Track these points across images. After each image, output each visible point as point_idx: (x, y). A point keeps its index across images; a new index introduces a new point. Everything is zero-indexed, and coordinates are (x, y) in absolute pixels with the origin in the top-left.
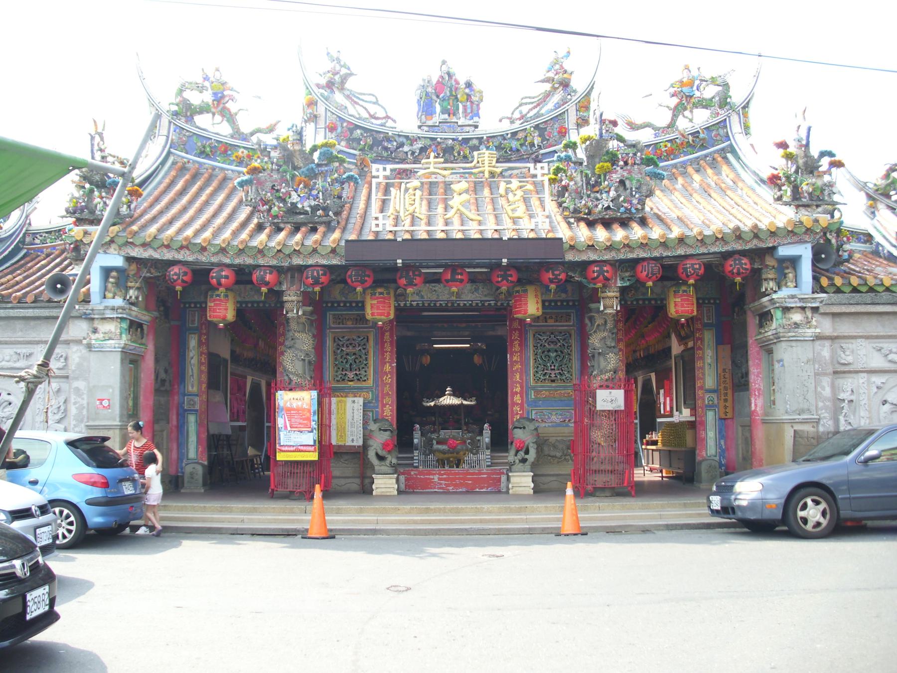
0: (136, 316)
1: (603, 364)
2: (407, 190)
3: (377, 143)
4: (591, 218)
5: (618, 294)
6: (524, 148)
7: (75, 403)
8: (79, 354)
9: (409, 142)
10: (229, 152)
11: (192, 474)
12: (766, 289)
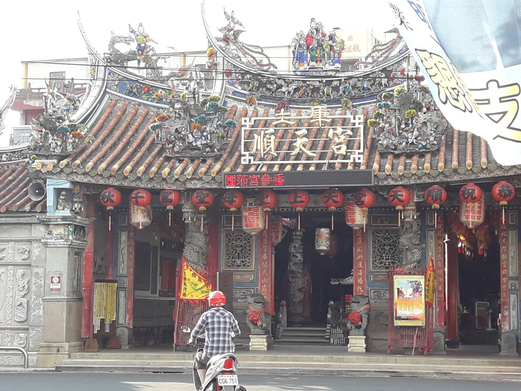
0: (80, 222)
1: (410, 256)
2: (265, 135)
3: (262, 85)
4: (396, 152)
5: (414, 208)
6: (374, 87)
7: (35, 284)
9: (286, 84)
10: (151, 92)
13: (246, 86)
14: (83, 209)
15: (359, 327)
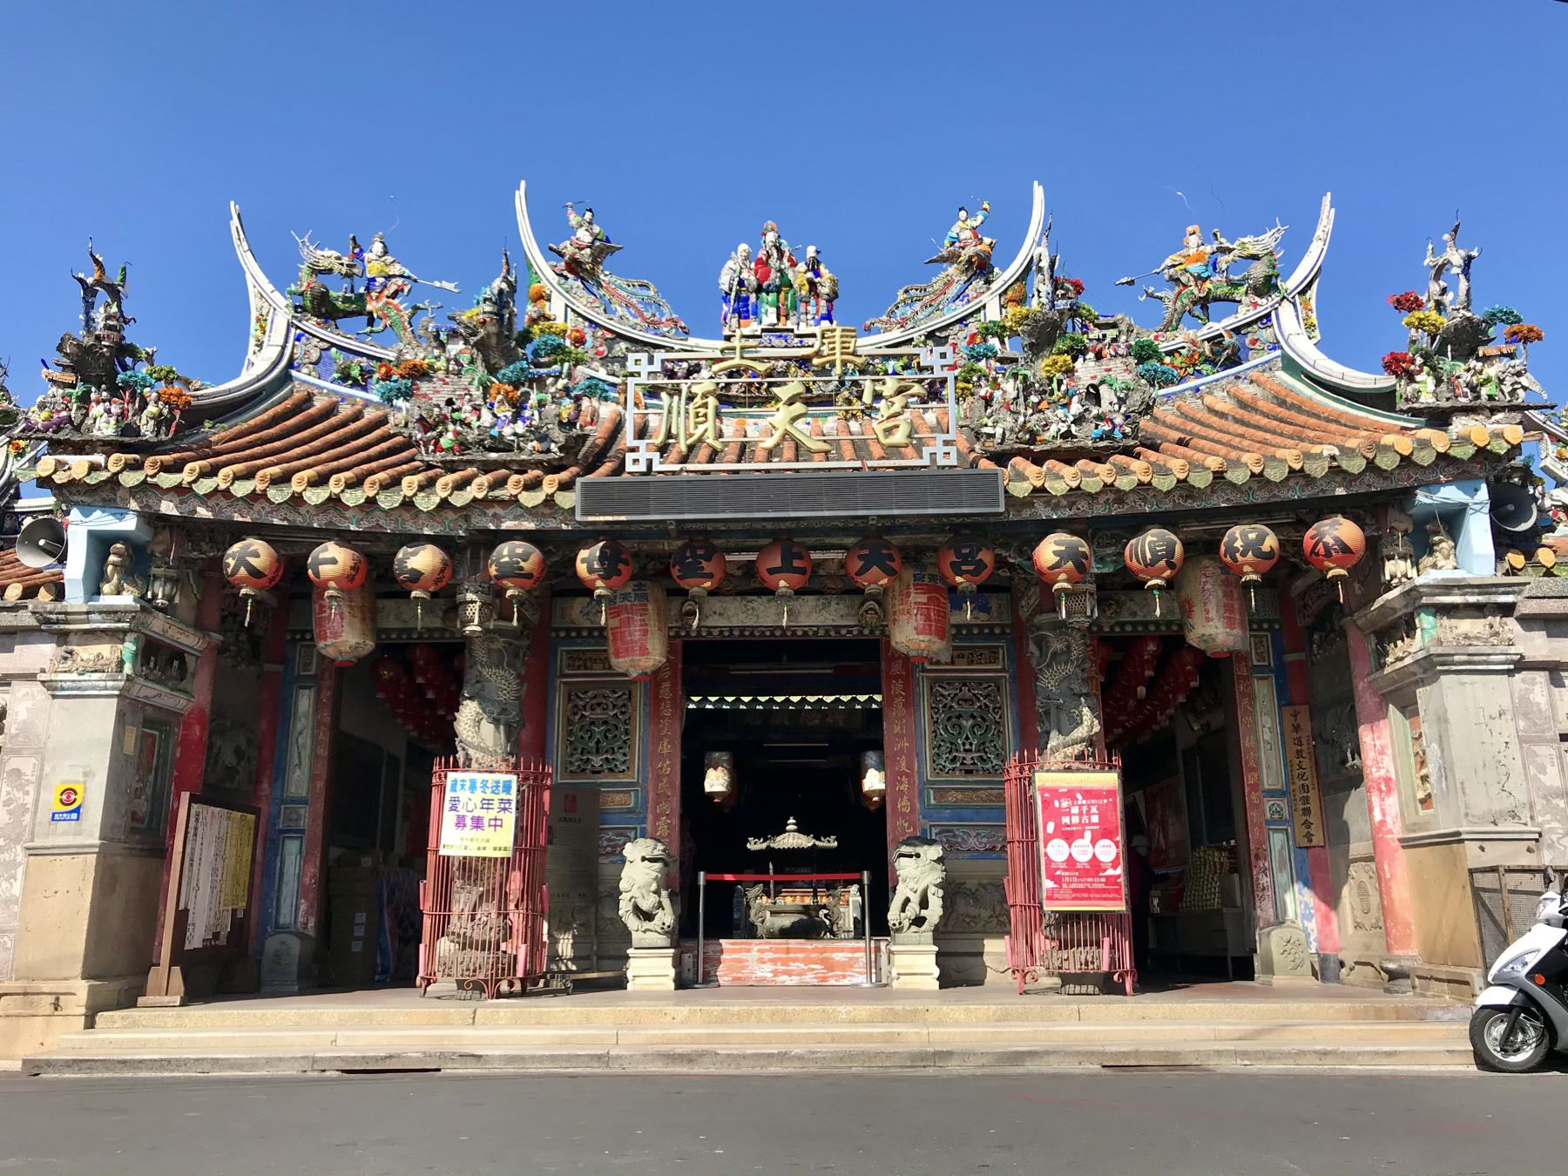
4: (1037, 448)
8: (29, 704)
11: (277, 955)
12: (1393, 577)
13: (616, 367)
14: (177, 600)
15: (919, 921)
